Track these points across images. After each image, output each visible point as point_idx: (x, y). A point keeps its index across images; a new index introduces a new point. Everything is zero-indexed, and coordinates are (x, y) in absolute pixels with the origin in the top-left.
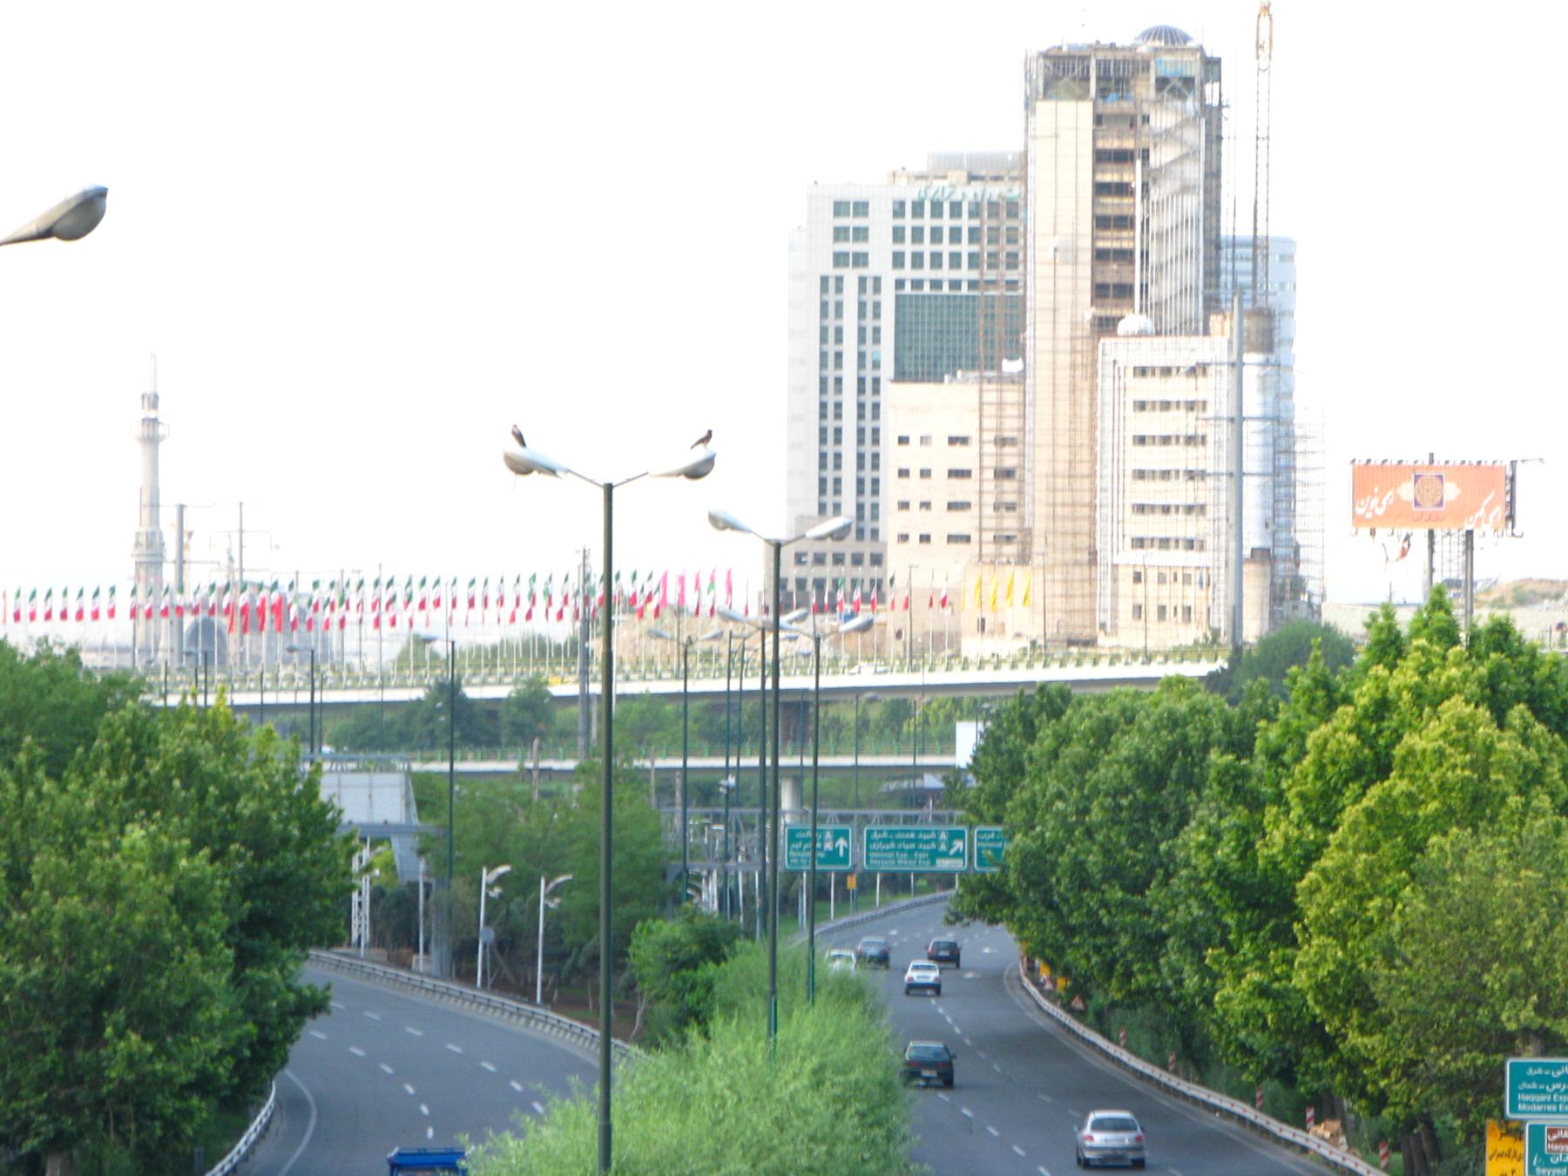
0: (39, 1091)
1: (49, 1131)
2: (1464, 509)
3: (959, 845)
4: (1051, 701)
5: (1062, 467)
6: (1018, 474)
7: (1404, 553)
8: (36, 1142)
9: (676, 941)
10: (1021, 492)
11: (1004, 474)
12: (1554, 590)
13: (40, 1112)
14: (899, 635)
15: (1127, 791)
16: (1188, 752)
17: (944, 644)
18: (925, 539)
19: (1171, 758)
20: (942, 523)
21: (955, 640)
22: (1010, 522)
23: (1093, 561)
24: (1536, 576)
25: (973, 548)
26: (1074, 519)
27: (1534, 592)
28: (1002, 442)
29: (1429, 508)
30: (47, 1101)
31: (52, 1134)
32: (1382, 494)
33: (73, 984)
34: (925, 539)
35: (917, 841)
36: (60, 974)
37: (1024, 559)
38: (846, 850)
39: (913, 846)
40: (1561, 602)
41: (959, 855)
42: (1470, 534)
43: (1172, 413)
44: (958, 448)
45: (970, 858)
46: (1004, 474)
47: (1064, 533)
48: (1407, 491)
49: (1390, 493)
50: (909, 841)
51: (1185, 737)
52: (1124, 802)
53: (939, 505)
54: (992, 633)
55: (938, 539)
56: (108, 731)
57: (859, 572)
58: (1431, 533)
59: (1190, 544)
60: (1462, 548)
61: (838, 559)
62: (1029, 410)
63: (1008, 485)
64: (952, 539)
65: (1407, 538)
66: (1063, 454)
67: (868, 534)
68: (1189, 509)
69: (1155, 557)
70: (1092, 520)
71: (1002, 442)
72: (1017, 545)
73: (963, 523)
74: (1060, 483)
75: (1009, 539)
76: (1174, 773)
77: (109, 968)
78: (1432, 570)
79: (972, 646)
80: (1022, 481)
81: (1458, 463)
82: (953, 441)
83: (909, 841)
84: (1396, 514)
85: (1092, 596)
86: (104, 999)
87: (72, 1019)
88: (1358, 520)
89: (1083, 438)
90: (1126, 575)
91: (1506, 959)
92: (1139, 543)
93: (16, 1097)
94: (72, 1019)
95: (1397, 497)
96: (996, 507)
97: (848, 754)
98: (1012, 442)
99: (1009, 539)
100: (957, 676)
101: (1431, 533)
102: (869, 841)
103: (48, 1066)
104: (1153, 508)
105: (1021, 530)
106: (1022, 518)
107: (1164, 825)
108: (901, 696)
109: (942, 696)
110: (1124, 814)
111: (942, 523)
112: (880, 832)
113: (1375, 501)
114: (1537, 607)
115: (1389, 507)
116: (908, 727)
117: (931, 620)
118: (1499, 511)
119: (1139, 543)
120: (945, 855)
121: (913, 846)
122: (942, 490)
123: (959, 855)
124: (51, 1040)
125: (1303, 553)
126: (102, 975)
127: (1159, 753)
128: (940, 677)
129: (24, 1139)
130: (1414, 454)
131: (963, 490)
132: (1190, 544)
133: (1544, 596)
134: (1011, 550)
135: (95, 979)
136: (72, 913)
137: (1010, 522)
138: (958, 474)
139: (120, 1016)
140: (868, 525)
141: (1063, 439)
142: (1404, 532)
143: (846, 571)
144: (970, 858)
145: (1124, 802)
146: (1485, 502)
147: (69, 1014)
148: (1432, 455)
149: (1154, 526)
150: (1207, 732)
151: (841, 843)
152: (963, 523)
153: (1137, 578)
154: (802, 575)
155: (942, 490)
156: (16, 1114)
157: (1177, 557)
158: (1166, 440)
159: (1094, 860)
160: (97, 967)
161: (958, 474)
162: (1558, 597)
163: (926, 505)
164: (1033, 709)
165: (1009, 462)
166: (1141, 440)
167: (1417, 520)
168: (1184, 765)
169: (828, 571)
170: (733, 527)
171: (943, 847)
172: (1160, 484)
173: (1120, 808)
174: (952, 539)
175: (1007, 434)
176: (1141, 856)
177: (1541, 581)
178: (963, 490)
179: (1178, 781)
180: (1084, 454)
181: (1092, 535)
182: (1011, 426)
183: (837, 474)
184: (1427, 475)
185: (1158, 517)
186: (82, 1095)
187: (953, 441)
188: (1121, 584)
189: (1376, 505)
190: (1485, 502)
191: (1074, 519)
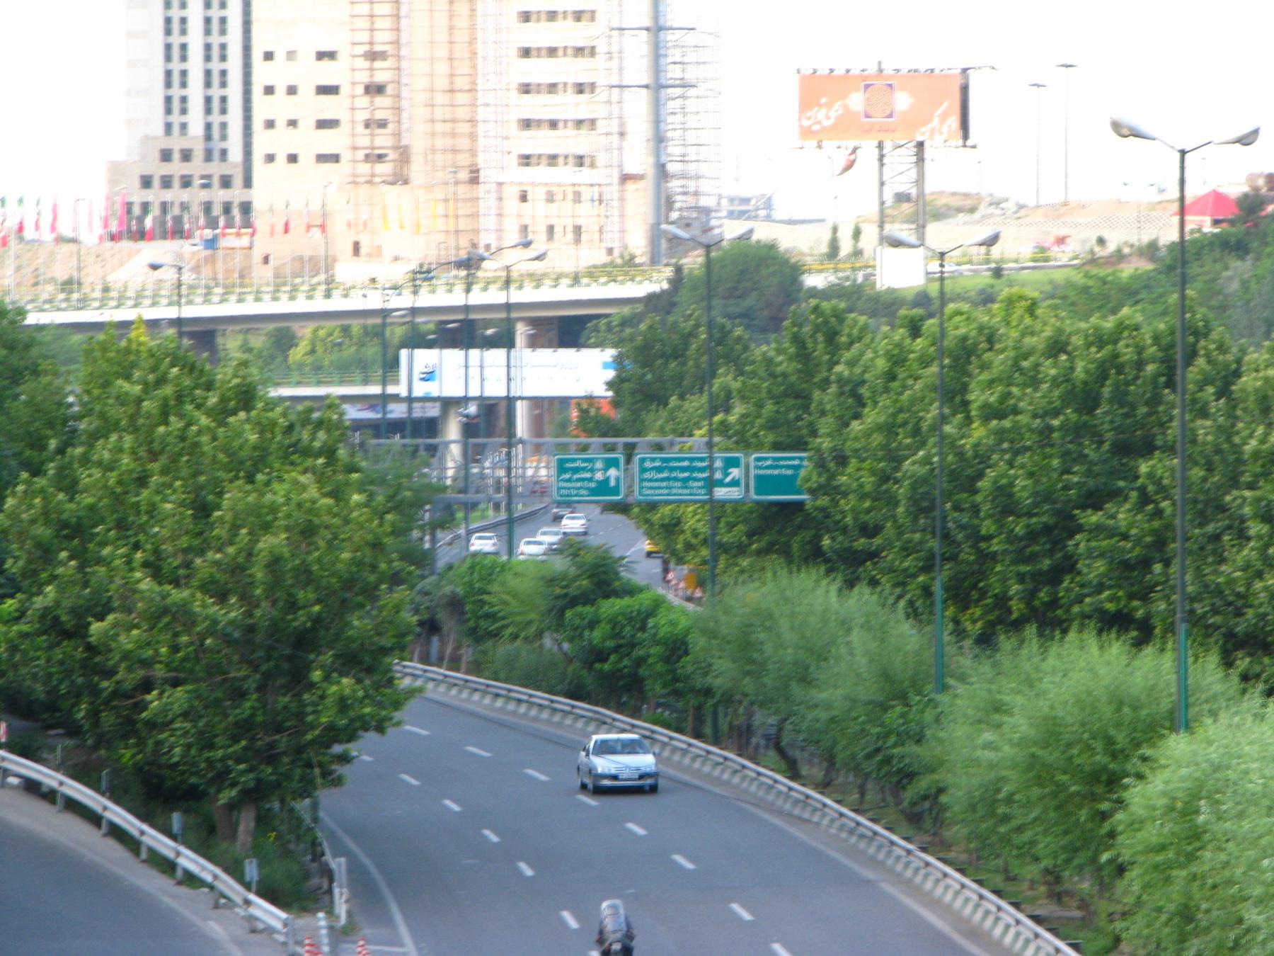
0: (235, 739)
1: (248, 780)
2: (918, 118)
3: (735, 473)
4: (826, 322)
5: (442, 83)
6: (390, 89)
7: (850, 166)
8: (234, 793)
9: (563, 576)
10: (397, 109)
11: (375, 89)
12: (968, 203)
13: (239, 761)
14: (266, 260)
15: (1056, 413)
16: (1120, 369)
17: (318, 268)
18: (293, 158)
19: (1102, 377)
20: (310, 142)
21: (329, 263)
22: (383, 140)
23: (474, 180)
24: (950, 188)
25: (344, 168)
26: (453, 135)
27: (947, 206)
28: (373, 56)
29: (878, 120)
30: (245, 749)
31: (252, 784)
32: (829, 106)
33: (275, 628)
34: (293, 158)
35: (691, 469)
36: (264, 612)
37: (400, 179)
38: (618, 479)
39: (686, 475)
40: (977, 215)
41: (735, 483)
42: (920, 145)
43: (559, 23)
44: (326, 63)
45: (747, 486)
46: (375, 89)
47: (445, 151)
48: (856, 101)
49: (837, 105)
50: (683, 469)
51: (1116, 356)
52: (1056, 423)
53: (307, 123)
54: (370, 255)
55: (307, 159)
56: (151, 361)
57: (168, 195)
58: (880, 146)
59: (580, 161)
60: (914, 159)
61: (166, 183)
62: (404, 22)
63: (380, 101)
64: (322, 158)
65: (855, 150)
66: (442, 68)
67: (216, 155)
68: (579, 123)
69: (540, 173)
70: (473, 137)
71: (373, 56)
72: (396, 165)
73: (330, 141)
74: (441, 99)
75: (380, 157)
76: (1106, 391)
77: (317, 608)
78: (882, 184)
79: (348, 270)
80: (398, 96)
81: (842, 72)
82: (321, 56)
83: (683, 469)
84: (843, 126)
85: (475, 216)
86: (305, 641)
87: (272, 663)
88: (806, 133)
89: (461, 51)
90: (511, 193)
91: (250, 604)
92: (526, 160)
93: (211, 746)
94: (272, 663)
95: (845, 107)
96: (367, 125)
97: (375, 383)
98: (382, 56)
99: (380, 157)
100: (337, 304)
101: (880, 146)
102: (643, 470)
103: (248, 712)
104: (539, 122)
105: (395, 148)
106: (397, 135)
107: (1099, 448)
108: (285, 324)
109: (330, 324)
110: (1055, 435)
111: (310, 142)
112: (653, 460)
113: (823, 111)
114: (951, 220)
115: (838, 118)
116: (297, 354)
117: (308, 243)
118: (954, 121)
119: (526, 160)
120: (721, 484)
121: (686, 475)
122: (311, 107)
123: (735, 483)
124: (251, 684)
125: (482, 174)
126: (309, 615)
127: (1087, 371)
128: (319, 304)
129: (219, 791)
130: (862, 62)
131: (329, 107)
132: (580, 161)
133: (959, 210)
134: (384, 169)
135: (301, 619)
136: (277, 551)
137: (383, 140)
138: (327, 90)
139: (327, 657)
140: (217, 145)
141: (443, 52)
142: (852, 144)
143: (196, 196)
144: (747, 486)
145: (1056, 423)
146: (939, 111)
147: (269, 658)
148: (880, 63)
149: (541, 142)
150: (1140, 350)
151: (612, 472)
152: (330, 141)
153: (524, 198)
154: (227, 199)
155: (311, 107)
156: (210, 762)
157: (565, 174)
158: (552, 52)
159: (1022, 485)
160: (304, 607)
161: (327, 90)
162: (972, 210)
163: (293, 123)
164: (807, 329)
165: (380, 77)
166: (526, 53)
167: (867, 131)
168: (1116, 385)
169: (175, 195)
170: (1137, 135)
171: (718, 475)
172: (545, 98)
173: (1051, 429)
174: (322, 158)
175: (377, 48)
176: (1076, 479)
177: (954, 194)
178: (329, 107)
179: (1111, 401)
180: (463, 68)
181: (473, 153)
182: (383, 39)
183: (223, 92)
184: (877, 83)
185: (545, 133)
186: (283, 741)
187: (321, 56)
188: (506, 203)
189: (824, 116)
190: (939, 111)
191: (453, 135)
